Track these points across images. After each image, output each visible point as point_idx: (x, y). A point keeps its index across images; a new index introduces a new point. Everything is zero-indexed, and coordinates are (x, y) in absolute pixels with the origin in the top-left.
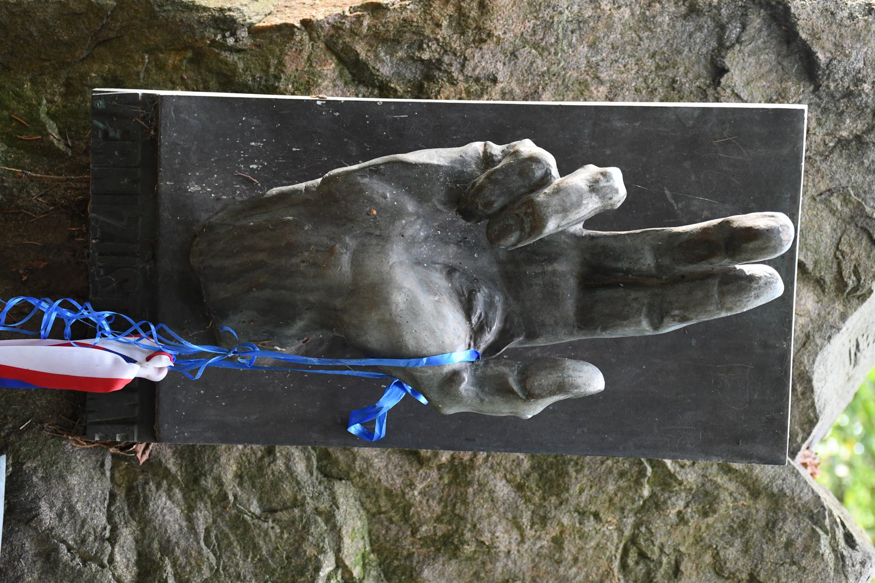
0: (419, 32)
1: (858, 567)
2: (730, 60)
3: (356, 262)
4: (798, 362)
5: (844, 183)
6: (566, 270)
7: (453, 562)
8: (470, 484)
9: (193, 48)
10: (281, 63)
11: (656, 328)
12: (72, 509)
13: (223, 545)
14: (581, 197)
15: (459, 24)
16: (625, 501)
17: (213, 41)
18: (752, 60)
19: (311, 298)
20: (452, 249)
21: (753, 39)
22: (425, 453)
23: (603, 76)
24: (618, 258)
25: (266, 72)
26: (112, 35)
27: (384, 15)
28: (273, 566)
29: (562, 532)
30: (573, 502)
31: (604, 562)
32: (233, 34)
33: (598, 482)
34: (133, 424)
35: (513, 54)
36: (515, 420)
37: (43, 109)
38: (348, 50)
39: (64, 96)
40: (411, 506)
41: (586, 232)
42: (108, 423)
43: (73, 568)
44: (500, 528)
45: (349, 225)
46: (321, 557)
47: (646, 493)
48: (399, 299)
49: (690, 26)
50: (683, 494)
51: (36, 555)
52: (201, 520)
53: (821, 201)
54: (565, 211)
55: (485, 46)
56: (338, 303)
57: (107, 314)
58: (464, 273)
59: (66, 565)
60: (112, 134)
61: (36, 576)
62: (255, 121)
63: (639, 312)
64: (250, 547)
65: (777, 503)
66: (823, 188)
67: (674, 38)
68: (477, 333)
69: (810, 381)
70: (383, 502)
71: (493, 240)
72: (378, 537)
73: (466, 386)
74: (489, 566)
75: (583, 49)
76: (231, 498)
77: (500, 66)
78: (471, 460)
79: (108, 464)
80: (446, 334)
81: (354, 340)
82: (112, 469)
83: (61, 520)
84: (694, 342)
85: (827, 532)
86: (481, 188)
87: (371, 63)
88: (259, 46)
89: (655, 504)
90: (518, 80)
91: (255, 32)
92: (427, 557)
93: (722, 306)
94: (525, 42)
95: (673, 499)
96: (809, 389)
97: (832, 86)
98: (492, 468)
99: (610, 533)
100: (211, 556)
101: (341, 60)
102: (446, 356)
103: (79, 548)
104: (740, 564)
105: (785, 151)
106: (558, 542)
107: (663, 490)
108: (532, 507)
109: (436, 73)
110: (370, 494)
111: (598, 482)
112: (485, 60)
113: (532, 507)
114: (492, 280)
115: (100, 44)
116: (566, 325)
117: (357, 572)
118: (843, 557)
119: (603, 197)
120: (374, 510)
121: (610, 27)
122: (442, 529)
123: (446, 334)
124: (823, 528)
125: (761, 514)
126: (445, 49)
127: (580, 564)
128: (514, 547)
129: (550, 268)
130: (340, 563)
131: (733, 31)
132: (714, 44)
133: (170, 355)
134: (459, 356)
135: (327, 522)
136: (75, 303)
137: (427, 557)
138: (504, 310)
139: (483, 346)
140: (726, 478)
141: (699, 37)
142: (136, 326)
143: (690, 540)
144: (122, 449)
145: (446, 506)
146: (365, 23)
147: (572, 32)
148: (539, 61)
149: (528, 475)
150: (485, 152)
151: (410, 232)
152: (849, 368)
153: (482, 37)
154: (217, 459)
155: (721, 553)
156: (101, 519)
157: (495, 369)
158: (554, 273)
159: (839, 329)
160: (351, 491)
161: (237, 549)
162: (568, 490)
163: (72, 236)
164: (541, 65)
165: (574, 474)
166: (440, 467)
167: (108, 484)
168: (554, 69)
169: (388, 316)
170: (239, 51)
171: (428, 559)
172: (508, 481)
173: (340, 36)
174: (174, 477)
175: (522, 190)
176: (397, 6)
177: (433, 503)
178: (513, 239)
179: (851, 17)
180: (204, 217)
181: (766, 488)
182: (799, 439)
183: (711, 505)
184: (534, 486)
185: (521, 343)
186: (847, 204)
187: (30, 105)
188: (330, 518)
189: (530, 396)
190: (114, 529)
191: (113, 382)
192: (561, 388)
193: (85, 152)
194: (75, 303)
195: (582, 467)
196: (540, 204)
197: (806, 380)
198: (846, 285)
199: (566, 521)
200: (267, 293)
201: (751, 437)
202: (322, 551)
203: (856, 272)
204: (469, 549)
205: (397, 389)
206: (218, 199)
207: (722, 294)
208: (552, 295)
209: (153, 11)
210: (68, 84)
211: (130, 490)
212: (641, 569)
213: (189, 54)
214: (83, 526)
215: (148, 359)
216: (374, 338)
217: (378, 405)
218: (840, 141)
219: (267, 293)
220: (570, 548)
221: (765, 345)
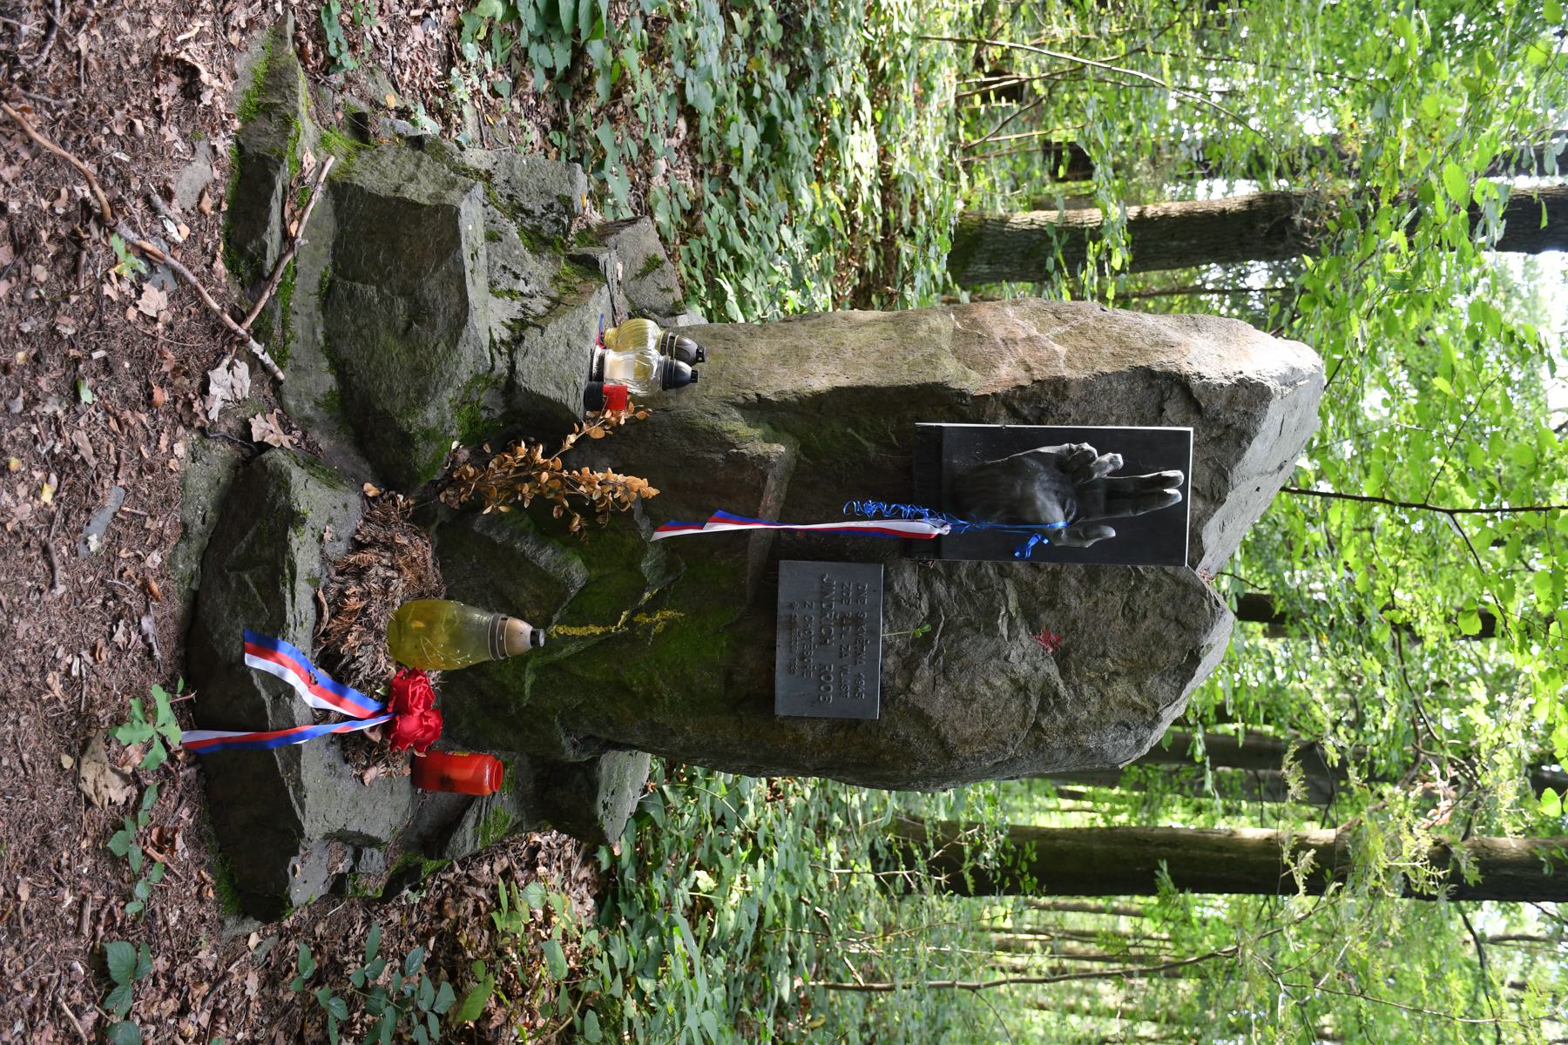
6: (1100, 491)
22: (1042, 565)
36: (1082, 548)
48: (1039, 503)
64: (972, 603)
68: (1066, 516)
81: (1022, 516)
89: (1136, 588)
91: (973, 397)
99: (1117, 600)
103: (908, 601)
106: (1096, 603)
110: (1019, 584)
112: (1066, 407)
126: (1050, 403)
134: (1061, 524)
153: (1065, 398)
186: (134, 774)
188: (1003, 592)
189: (1088, 539)
192: (1099, 535)
216: (1029, 517)
220: (1101, 606)
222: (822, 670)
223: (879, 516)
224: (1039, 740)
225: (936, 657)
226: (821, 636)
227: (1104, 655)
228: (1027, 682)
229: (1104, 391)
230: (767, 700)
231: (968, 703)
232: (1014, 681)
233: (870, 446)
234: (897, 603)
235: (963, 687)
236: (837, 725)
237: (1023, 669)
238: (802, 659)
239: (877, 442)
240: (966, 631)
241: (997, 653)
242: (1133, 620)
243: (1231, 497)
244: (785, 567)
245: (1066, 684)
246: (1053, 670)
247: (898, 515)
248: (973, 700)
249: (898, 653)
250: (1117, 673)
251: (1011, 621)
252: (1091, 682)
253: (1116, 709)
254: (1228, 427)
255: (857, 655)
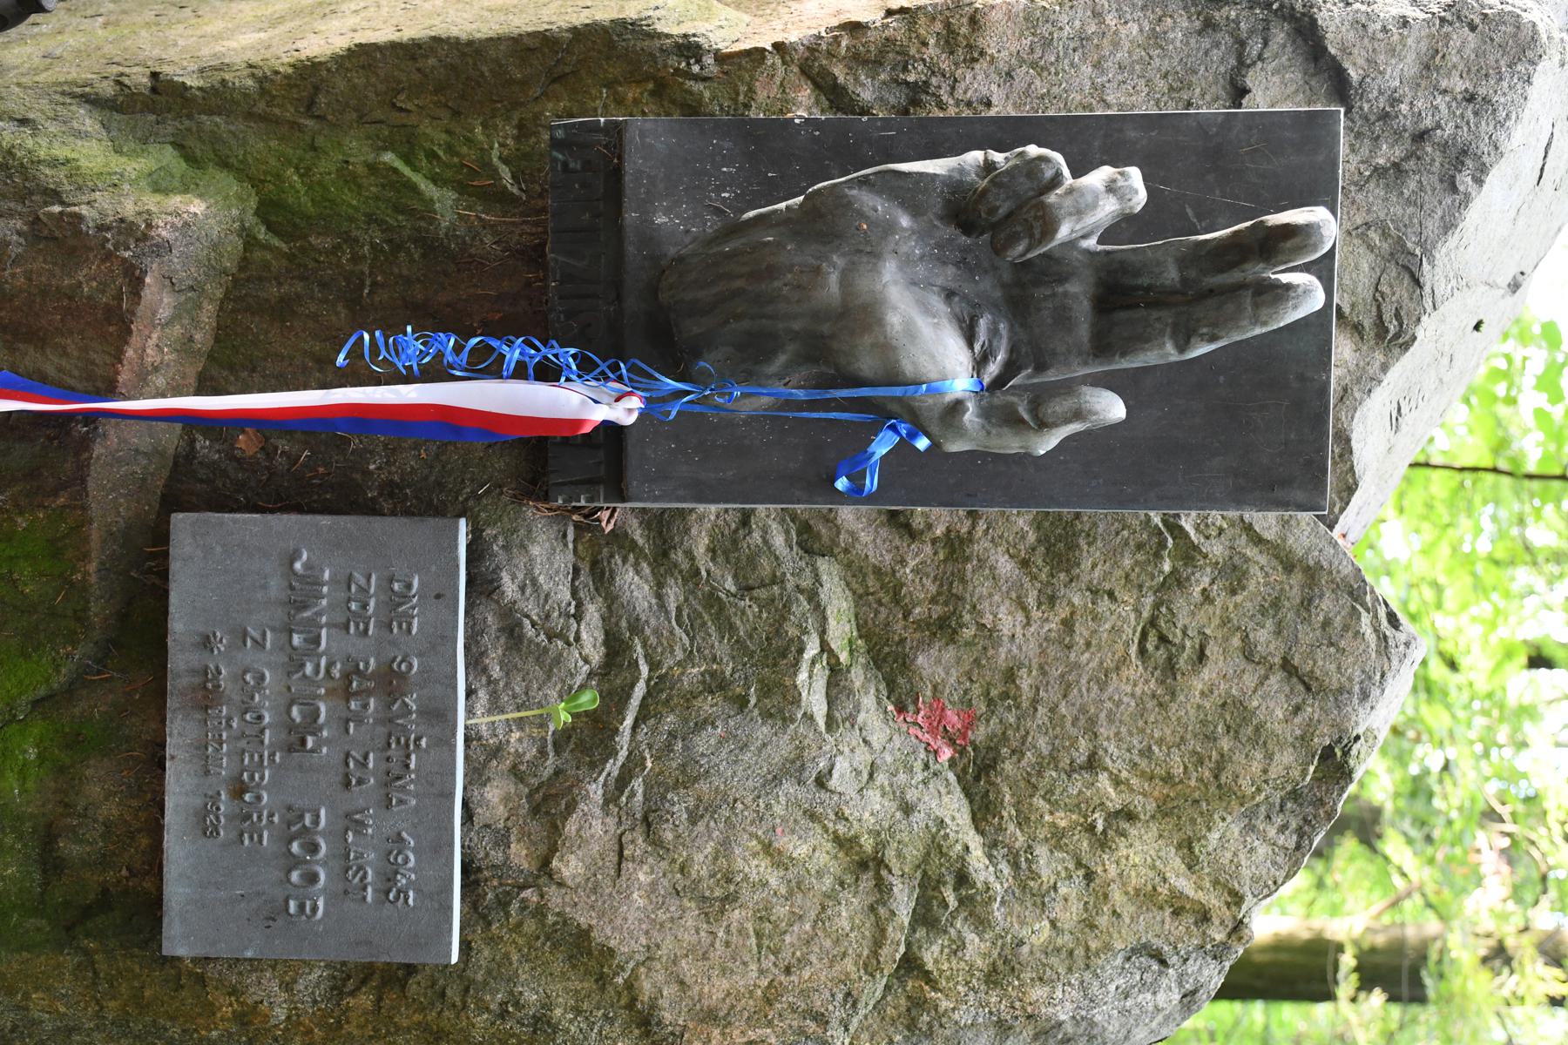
0: (903, 52)
1: (1402, 648)
2: (1252, 79)
3: (845, 282)
4: (1337, 419)
5: (1382, 215)
6: (1079, 291)
7: (951, 648)
8: (968, 559)
9: (655, 79)
10: (751, 90)
11: (1182, 350)
12: (534, 581)
13: (696, 626)
14: (1097, 197)
15: (947, 42)
16: (1143, 577)
17: (677, 70)
18: (1276, 79)
19: (796, 326)
20: (951, 270)
21: (1276, 56)
23: (1109, 98)
24: (1137, 273)
25: (735, 100)
26: (567, 69)
27: (864, 34)
28: (752, 648)
29: (1072, 614)
30: (1085, 578)
31: (1120, 647)
32: (698, 61)
33: (1113, 555)
34: (598, 483)
35: (1008, 74)
37: (495, 153)
38: (826, 73)
39: (517, 139)
40: (902, 585)
41: (1100, 248)
42: (571, 483)
43: (538, 645)
44: (1002, 609)
45: (837, 242)
46: (805, 638)
47: (1167, 567)
48: (894, 320)
49: (1206, 43)
50: (1209, 570)
51: (499, 630)
52: (672, 598)
53: (1358, 236)
54: (1079, 213)
55: (977, 66)
56: (826, 328)
57: (573, 351)
58: (964, 298)
59: (530, 641)
60: (572, 165)
61: (500, 652)
62: (727, 144)
63: (1162, 333)
64: (726, 627)
65: (1312, 577)
66: (1359, 222)
67: (1189, 56)
68: (980, 363)
69: (1348, 440)
70: (871, 582)
71: (998, 250)
72: (866, 622)
73: (970, 416)
74: (991, 652)
75: (1087, 69)
76: (704, 573)
77: (994, 87)
78: (969, 533)
79: (570, 537)
80: (947, 361)
81: (853, 384)
82: (575, 541)
83: (523, 593)
84: (1222, 379)
85: (1368, 611)
86: (985, 191)
87: (851, 88)
88: (726, 73)
89: (1177, 581)
90: (1014, 104)
91: (721, 58)
92: (921, 642)
93: (1256, 321)
94: (1022, 62)
95: (1198, 575)
96: (1347, 450)
97: (1366, 107)
98: (993, 541)
100: (684, 636)
101: (817, 86)
102: (948, 383)
104: (1272, 647)
105: (1321, 158)
106: (1068, 624)
107: (1186, 565)
108: (1038, 585)
109: (923, 97)
110: (855, 571)
111: (1113, 555)
113: (1038, 585)
114: (996, 306)
115: (554, 81)
116: (1080, 354)
117: (844, 657)
118: (1385, 637)
119: (1121, 199)
120: (861, 591)
121: (1116, 45)
122: (937, 611)
123: (947, 361)
124: (1363, 604)
125: (1295, 590)
127: (1093, 649)
128: (1019, 630)
129: (1061, 290)
130: (825, 647)
131: (1254, 47)
132: (1233, 62)
133: (640, 397)
134: (961, 383)
135: (810, 600)
136: (538, 343)
137: (921, 642)
138: (1010, 339)
139: (986, 380)
140: (1256, 550)
141: (1216, 54)
142: (603, 367)
143: (1216, 621)
144: (586, 517)
145: (941, 585)
146: (844, 44)
147: (1074, 50)
148: (1038, 82)
149: (1034, 549)
150: (986, 160)
151: (904, 249)
152: (1390, 434)
153: (974, 55)
154: (687, 531)
155: (1251, 636)
156: (565, 594)
157: (1000, 398)
158: (1066, 294)
159: (1380, 382)
160: (836, 569)
161: (712, 630)
162: (1079, 565)
163: (528, 284)
164: (1040, 87)
165: (1085, 547)
166: (934, 541)
167: (571, 557)
168: (1055, 90)
169: (882, 340)
170: (705, 79)
171: (921, 645)
172: (1011, 557)
173: (816, 59)
174: (642, 550)
175: (1031, 193)
176: (878, 24)
177: (928, 582)
178: (1021, 248)
179: (1385, 29)
180: (672, 251)
181: (1300, 561)
182: (1336, 510)
183: (1239, 581)
184: (1040, 562)
185: (1029, 377)
187: (482, 149)
188: (813, 596)
189: (1043, 425)
190: (579, 605)
191: (580, 423)
192: (1078, 415)
193: (541, 196)
194: (538, 343)
195: (1095, 539)
196: (1051, 206)
197: (1344, 440)
198: (1387, 331)
199: (1076, 600)
200: (746, 324)
201: (1286, 483)
202: (805, 632)
203: (1398, 316)
204: (968, 633)
205: (890, 433)
206: (687, 231)
207: (1256, 306)
208: (1063, 319)
209: (611, 41)
210: (521, 126)
211: (595, 564)
212: (1162, 654)
213: (651, 86)
214: (546, 601)
215: (617, 400)
216: (866, 365)
217: (870, 450)
218: (1376, 169)
219: (746, 324)
221: (1302, 378)
222: (295, 826)
223: (435, 372)
224: (918, 1003)
225: (623, 781)
226: (291, 727)
227: (1093, 764)
228: (881, 846)
229: (1083, 38)
230: (147, 909)
231: (716, 905)
232: (845, 844)
233: (444, 202)
234: (512, 631)
235: (701, 864)
236: (350, 978)
237: (870, 810)
238: (239, 790)
239: (462, 188)
240: (708, 705)
241: (794, 767)
242: (1170, 667)
243: (1427, 331)
244: (188, 532)
245: (991, 846)
246: (953, 809)
247: (485, 366)
248: (730, 899)
249: (515, 773)
250: (1130, 816)
251: (836, 673)
252: (1057, 838)
253: (1127, 910)
254: (1421, 137)
255: (390, 780)
